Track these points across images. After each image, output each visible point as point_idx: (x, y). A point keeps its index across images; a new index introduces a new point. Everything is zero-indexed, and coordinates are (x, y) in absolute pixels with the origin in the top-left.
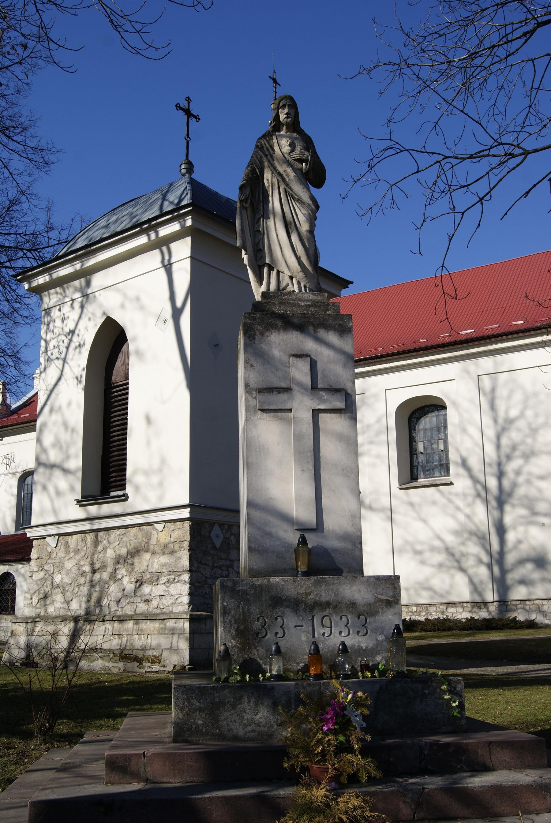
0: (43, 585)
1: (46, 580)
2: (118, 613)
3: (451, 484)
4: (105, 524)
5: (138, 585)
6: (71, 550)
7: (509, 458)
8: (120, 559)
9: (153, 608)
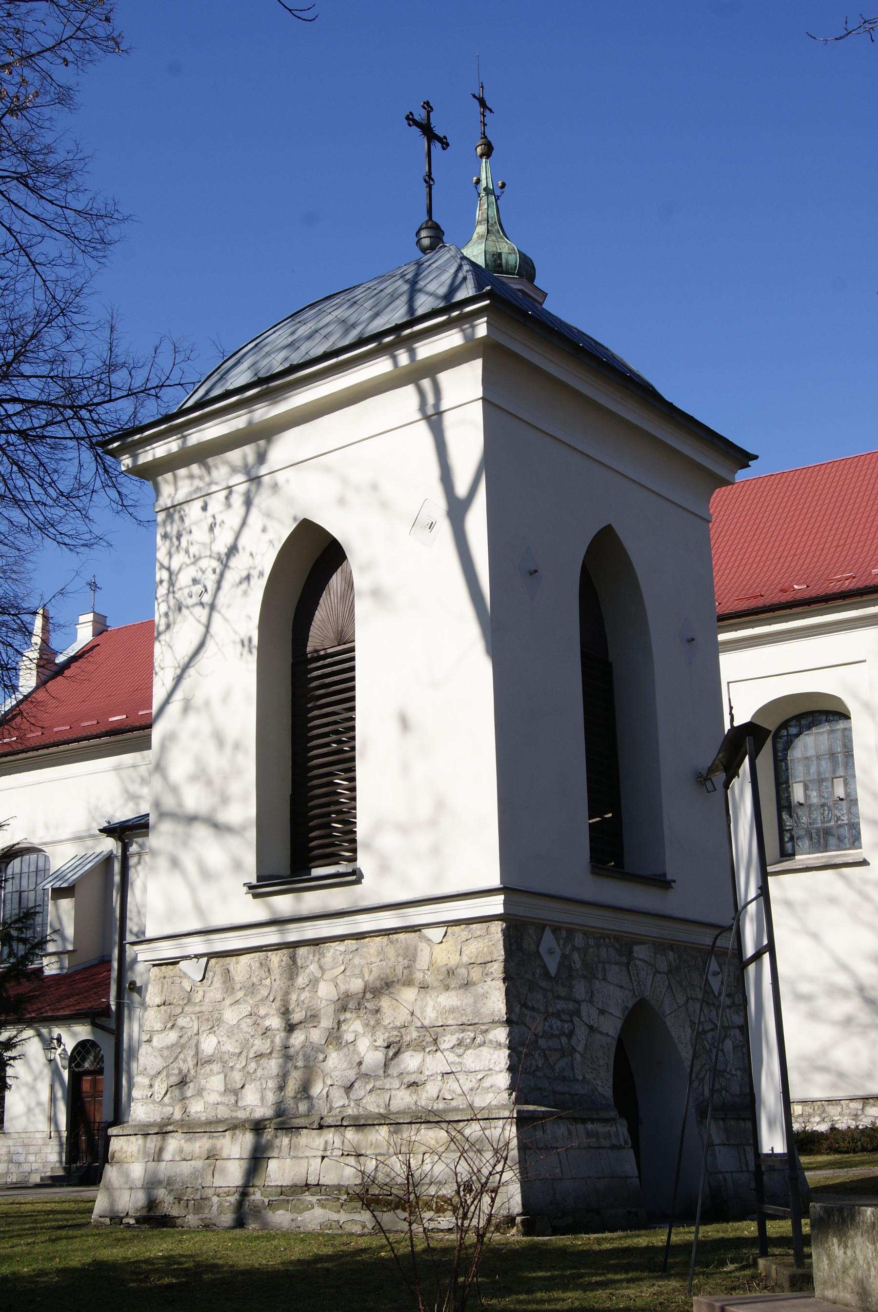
0: (176, 1058)
1: (183, 1047)
2: (350, 1111)
3: (864, 863)
4: (311, 931)
5: (391, 1054)
6: (238, 986)
8: (348, 1003)
9: (427, 1099)
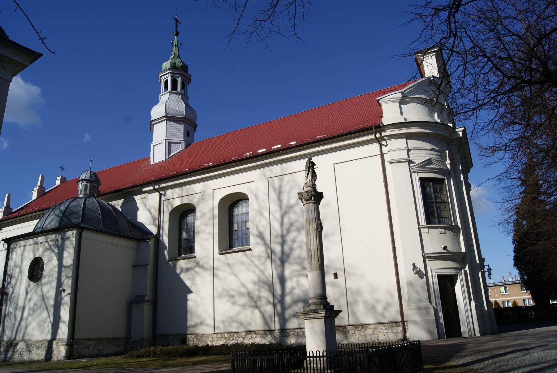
3: (250, 250)
7: (289, 231)
